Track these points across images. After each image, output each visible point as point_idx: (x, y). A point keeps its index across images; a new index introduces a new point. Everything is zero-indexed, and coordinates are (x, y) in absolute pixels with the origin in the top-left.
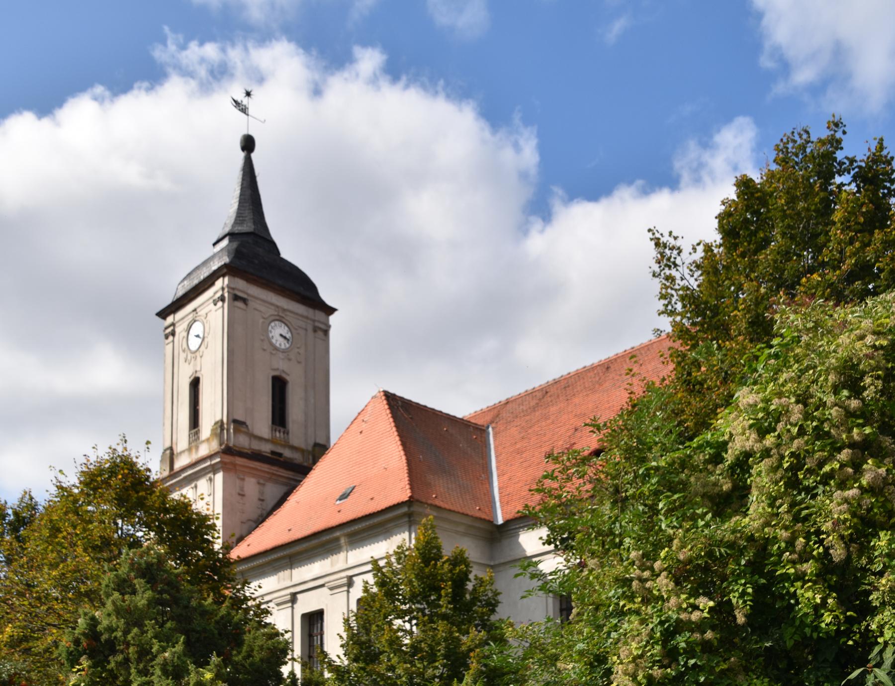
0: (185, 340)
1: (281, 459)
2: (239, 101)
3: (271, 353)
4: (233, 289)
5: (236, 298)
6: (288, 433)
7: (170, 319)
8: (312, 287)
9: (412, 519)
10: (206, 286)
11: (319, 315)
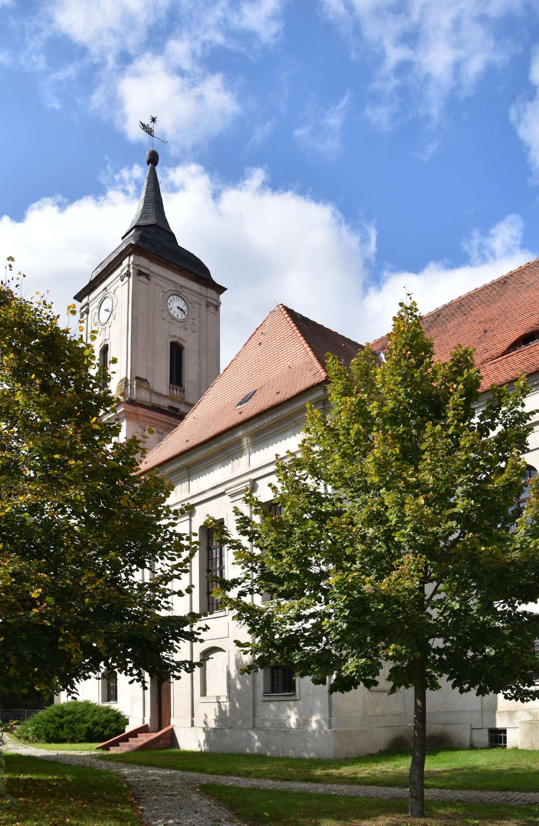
0: (97, 315)
1: (179, 414)
2: (146, 124)
3: (170, 322)
4: (138, 266)
5: (140, 273)
6: (184, 392)
7: (85, 301)
8: (206, 270)
9: (327, 406)
10: (115, 267)
11: (212, 293)
